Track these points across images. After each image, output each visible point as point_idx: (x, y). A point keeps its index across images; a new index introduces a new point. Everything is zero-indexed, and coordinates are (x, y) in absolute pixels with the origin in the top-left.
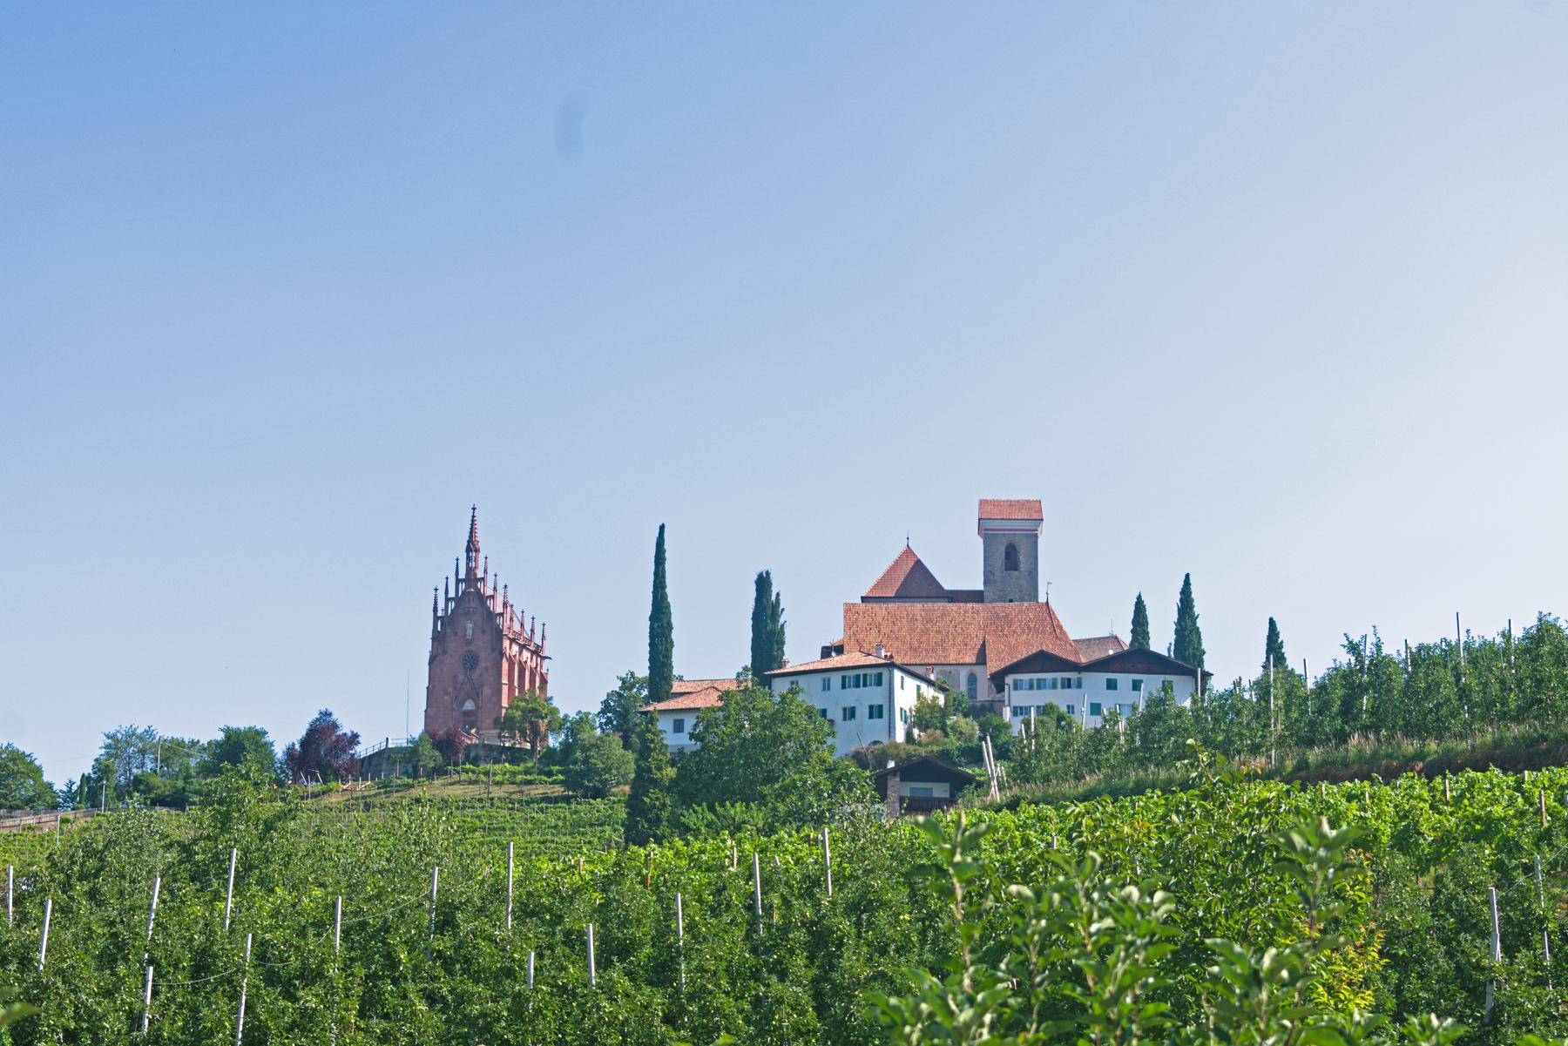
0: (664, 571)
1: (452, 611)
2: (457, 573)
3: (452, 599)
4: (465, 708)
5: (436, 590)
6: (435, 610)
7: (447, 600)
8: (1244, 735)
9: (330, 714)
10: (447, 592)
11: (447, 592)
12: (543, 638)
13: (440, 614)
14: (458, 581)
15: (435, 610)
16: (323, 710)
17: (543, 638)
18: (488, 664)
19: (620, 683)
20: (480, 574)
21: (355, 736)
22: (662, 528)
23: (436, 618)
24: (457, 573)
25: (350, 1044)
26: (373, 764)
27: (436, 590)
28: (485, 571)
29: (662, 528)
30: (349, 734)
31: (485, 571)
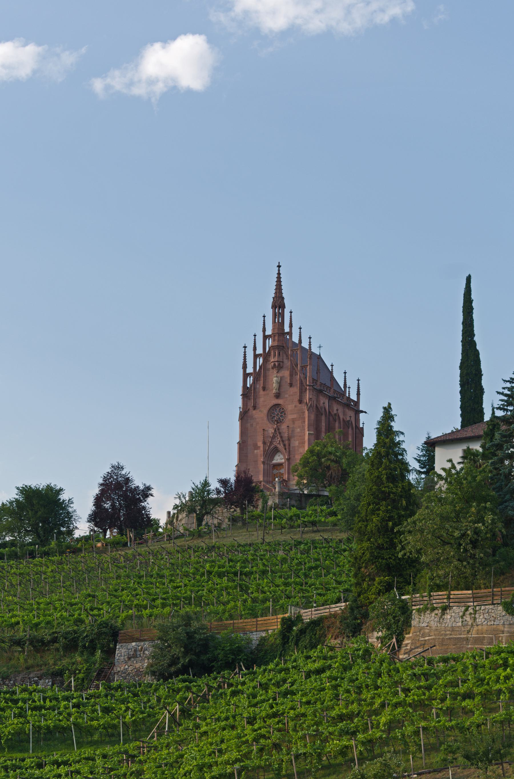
0: (472, 320)
1: (260, 367)
2: (264, 330)
3: (260, 355)
4: (274, 462)
5: (245, 347)
6: (245, 367)
7: (256, 356)
8: (93, 654)
9: (122, 468)
10: (255, 349)
11: (255, 349)
12: (358, 394)
13: (250, 369)
14: (265, 337)
15: (245, 367)
16: (115, 463)
17: (358, 394)
18: (295, 416)
19: (395, 429)
20: (287, 329)
21: (61, 490)
22: (469, 279)
23: (246, 375)
24: (264, 330)
25: (284, 776)
26: (179, 519)
27: (245, 347)
28: (291, 326)
29: (469, 279)
30: (142, 487)
31: (291, 326)
